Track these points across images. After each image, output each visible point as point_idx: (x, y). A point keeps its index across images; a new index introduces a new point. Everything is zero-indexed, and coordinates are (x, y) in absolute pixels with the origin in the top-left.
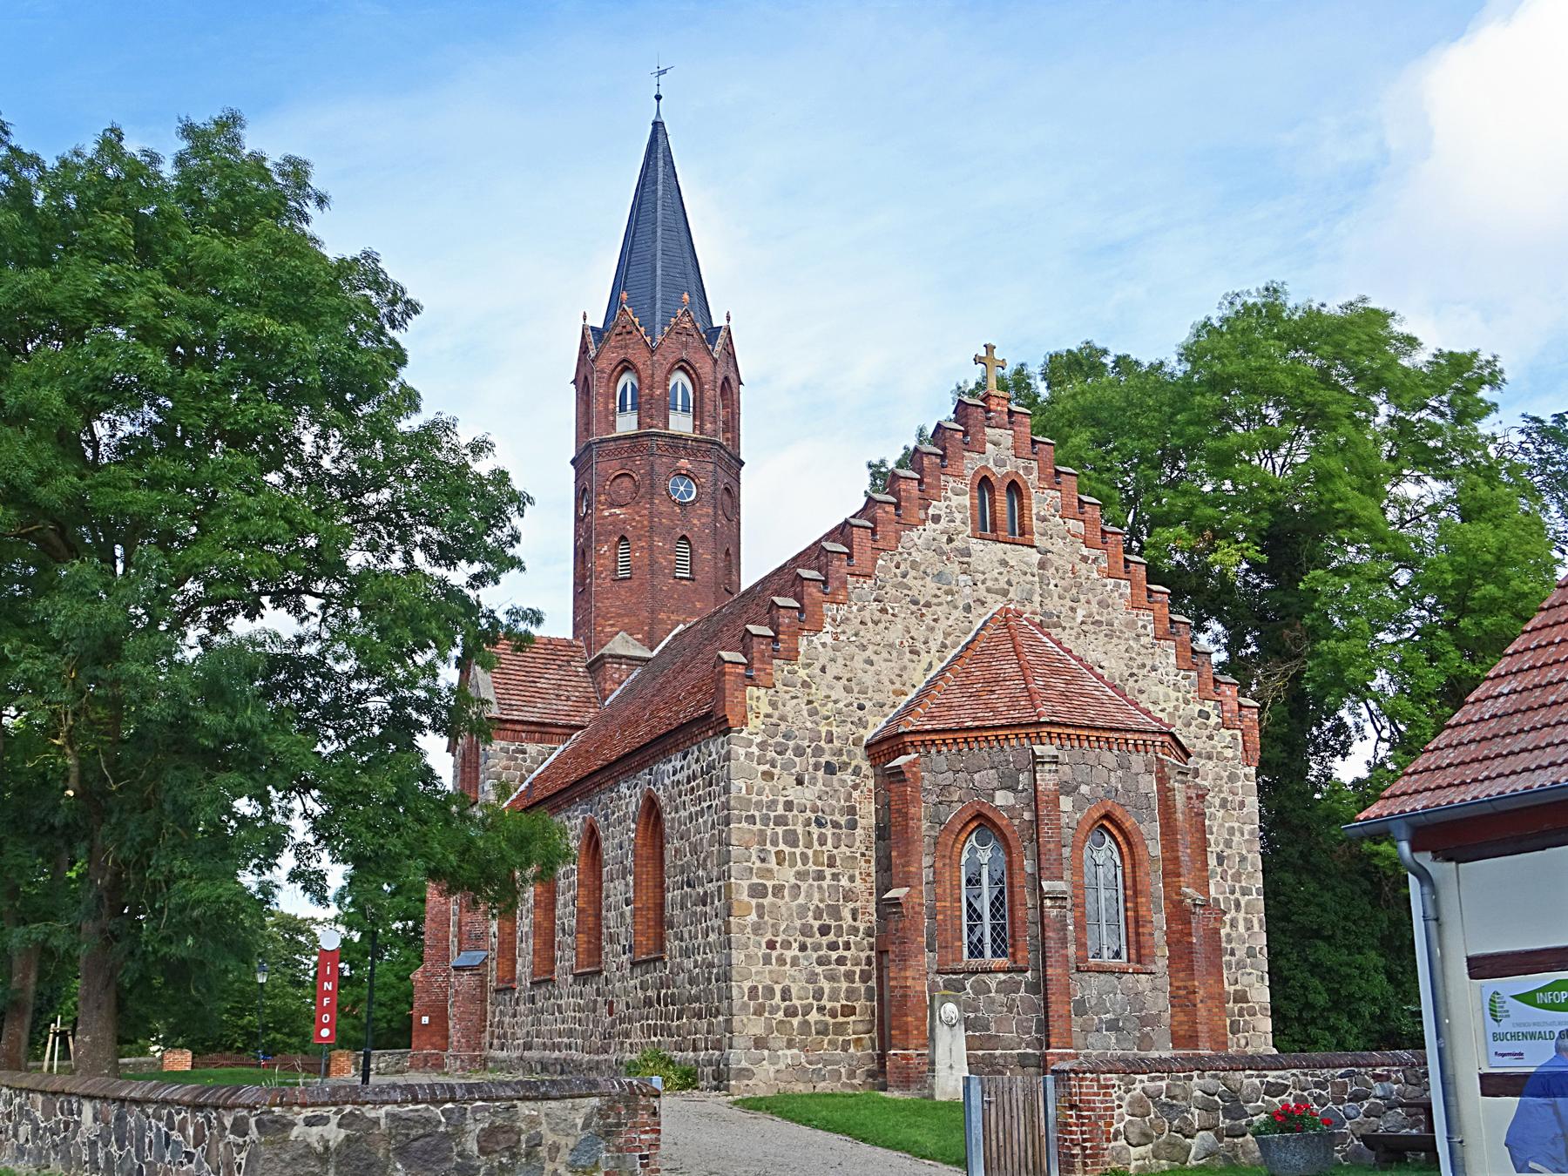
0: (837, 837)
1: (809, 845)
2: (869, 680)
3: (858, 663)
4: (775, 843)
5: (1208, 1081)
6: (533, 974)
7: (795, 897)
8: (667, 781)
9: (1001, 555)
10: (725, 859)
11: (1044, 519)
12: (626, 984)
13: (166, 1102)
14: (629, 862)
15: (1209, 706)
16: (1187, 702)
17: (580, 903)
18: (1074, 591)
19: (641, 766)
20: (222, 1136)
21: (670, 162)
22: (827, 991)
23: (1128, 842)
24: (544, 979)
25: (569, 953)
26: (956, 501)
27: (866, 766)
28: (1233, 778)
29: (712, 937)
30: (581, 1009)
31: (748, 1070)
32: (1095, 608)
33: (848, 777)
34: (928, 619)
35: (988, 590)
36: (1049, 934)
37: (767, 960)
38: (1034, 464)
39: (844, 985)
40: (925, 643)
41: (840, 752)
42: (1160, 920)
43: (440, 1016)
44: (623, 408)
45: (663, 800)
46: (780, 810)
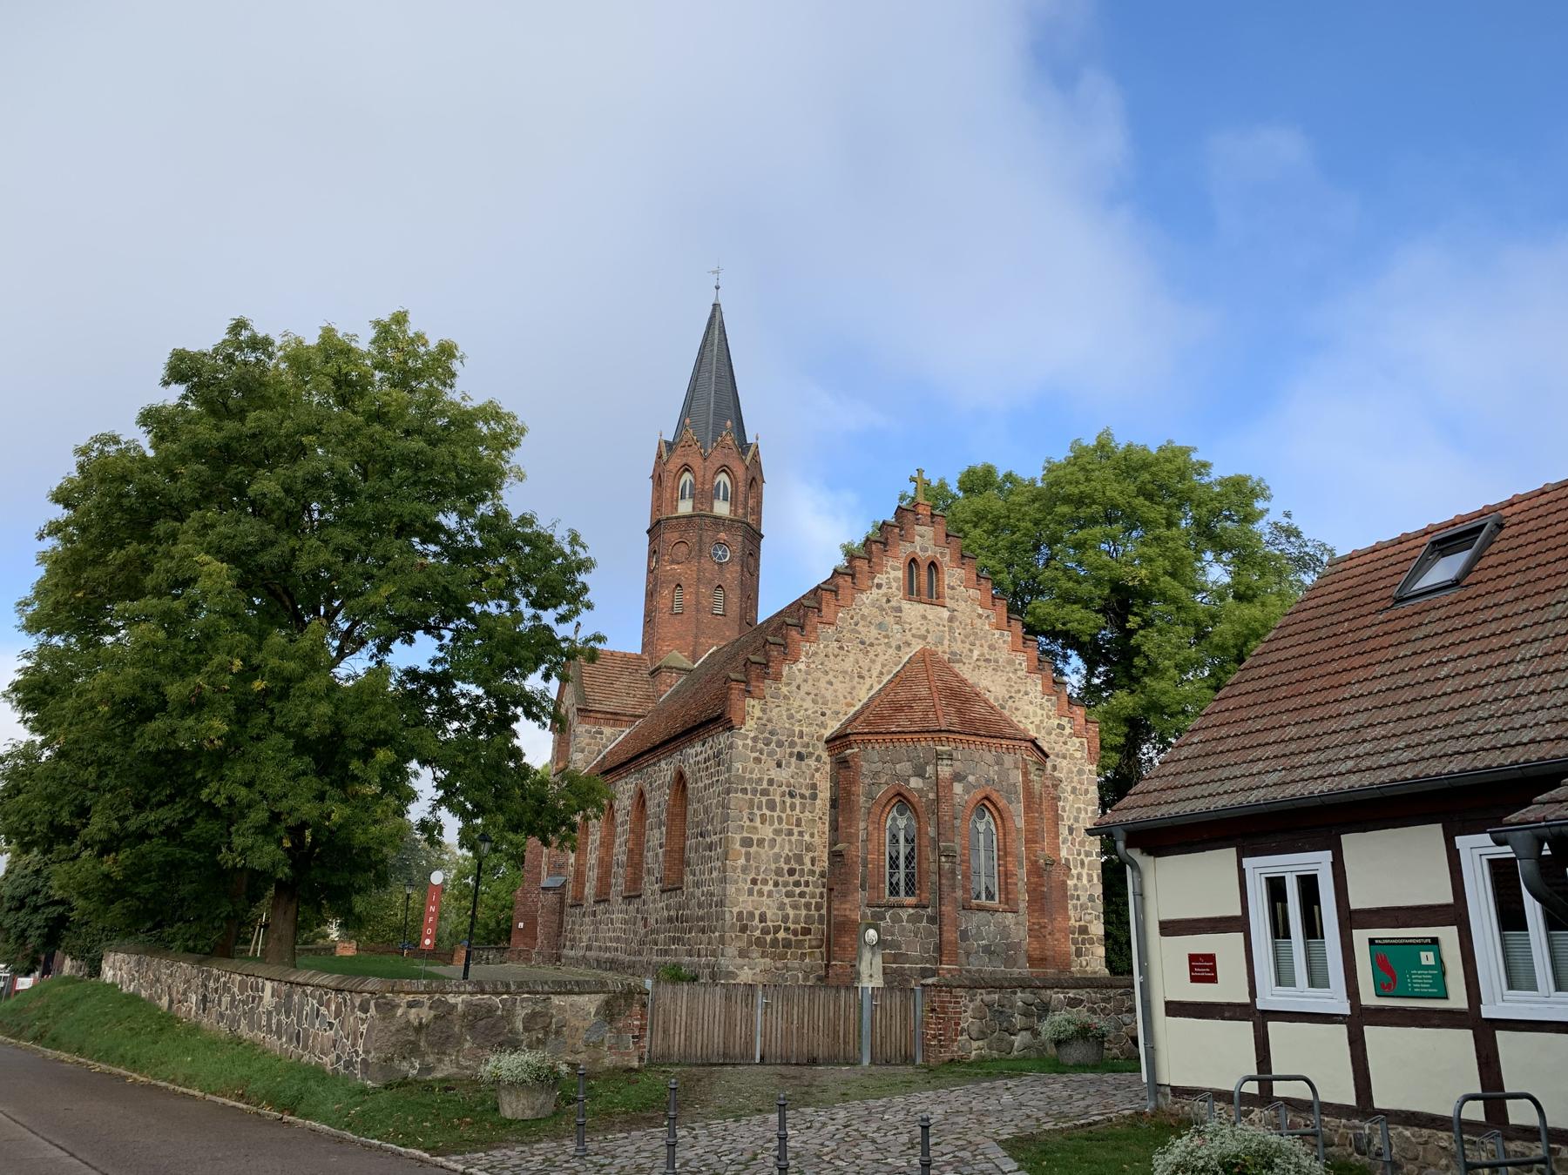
0: (803, 806)
1: (783, 810)
2: (829, 695)
3: (822, 684)
4: (760, 808)
7: (772, 847)
10: (726, 818)
11: (953, 588)
12: (657, 906)
13: (318, 986)
14: (664, 817)
15: (1064, 721)
16: (1049, 717)
23: (1001, 816)
25: (620, 880)
26: (893, 574)
27: (825, 756)
28: (1080, 772)
29: (715, 874)
30: (626, 922)
32: (986, 650)
33: (812, 762)
34: (871, 655)
37: (750, 892)
39: (804, 912)
41: (807, 745)
42: (1023, 873)
43: (532, 924)
46: (765, 785)
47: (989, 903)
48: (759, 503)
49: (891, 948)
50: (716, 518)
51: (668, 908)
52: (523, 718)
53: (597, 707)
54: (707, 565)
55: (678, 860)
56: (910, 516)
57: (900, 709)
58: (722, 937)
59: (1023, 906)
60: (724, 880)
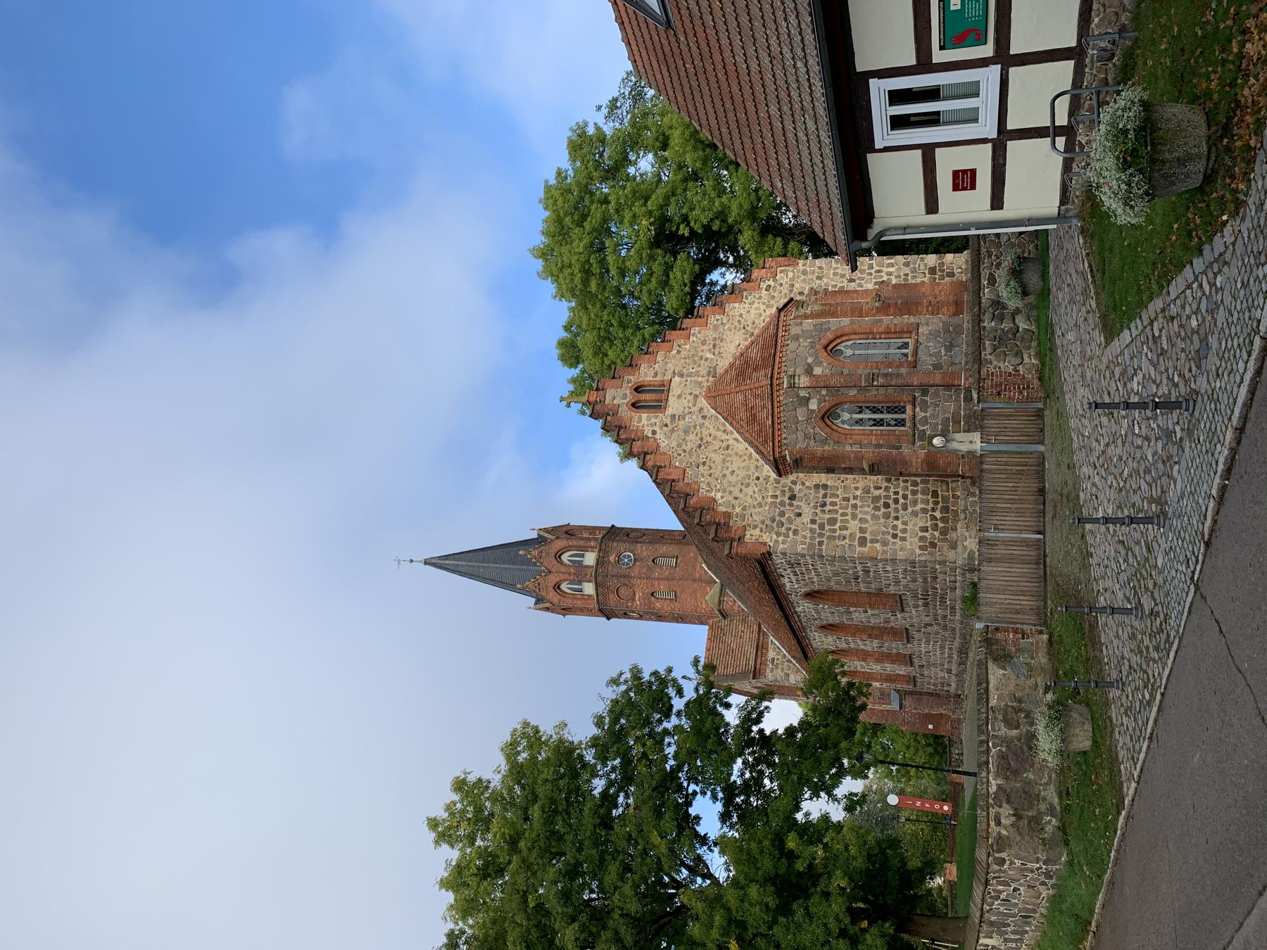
0: (833, 495)
1: (836, 512)
2: (742, 474)
3: (733, 479)
4: (834, 531)
5: (987, 317)
6: (906, 665)
7: (866, 521)
12: (914, 615)
13: (983, 900)
15: (764, 285)
16: (760, 298)
17: (865, 637)
19: (786, 599)
20: (1004, 872)
21: (447, 557)
23: (840, 336)
26: (644, 421)
27: (792, 477)
28: (805, 273)
29: (889, 568)
32: (706, 347)
33: (797, 488)
34: (710, 439)
37: (904, 539)
39: (919, 496)
41: (783, 492)
42: (886, 320)
43: (930, 718)
45: (807, 589)
46: (816, 526)
47: (911, 347)
49: (948, 426)
51: (916, 606)
52: (761, 726)
53: (752, 663)
55: (877, 598)
56: (598, 407)
57: (754, 417)
59: (912, 319)
60: (894, 561)
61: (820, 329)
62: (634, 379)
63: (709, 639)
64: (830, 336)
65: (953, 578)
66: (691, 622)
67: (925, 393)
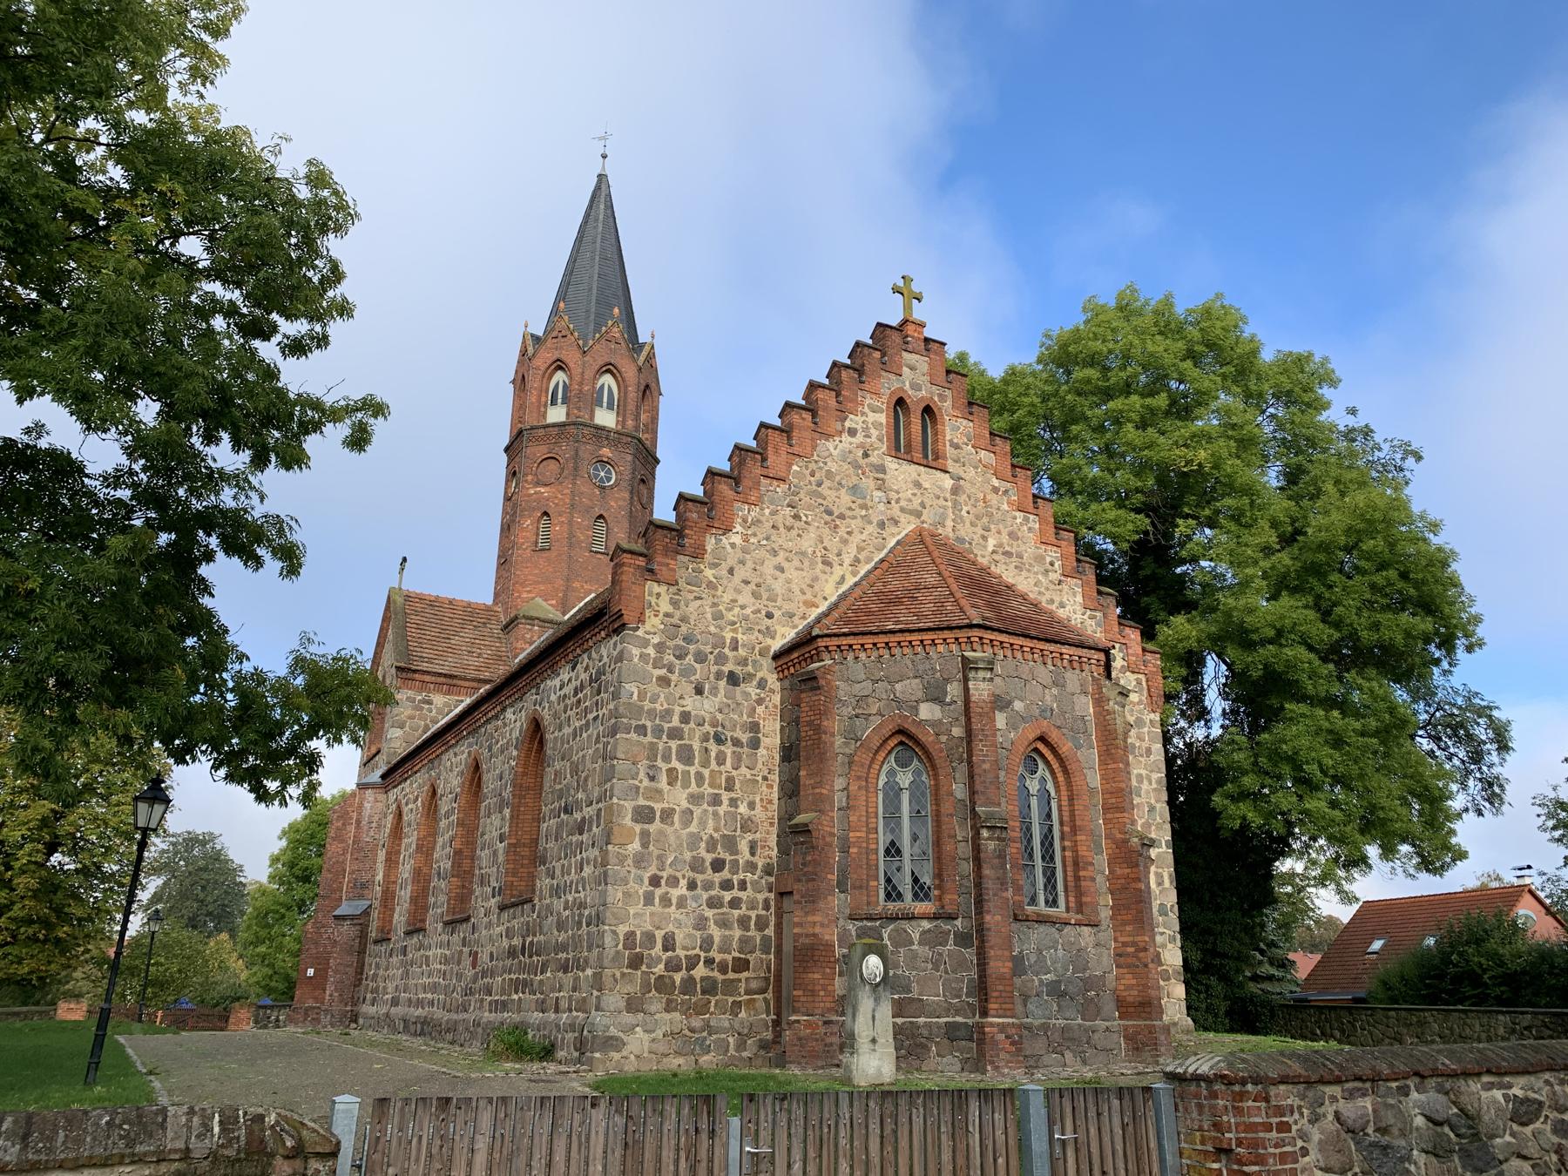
0: (738, 759)
1: (706, 764)
2: (778, 587)
4: (667, 759)
7: (687, 823)
8: (553, 698)
9: (914, 475)
10: (609, 775)
11: (957, 447)
12: (494, 931)
14: (507, 793)
18: (985, 520)
22: (717, 940)
23: (1064, 767)
24: (416, 928)
25: (442, 898)
26: (872, 417)
27: (773, 680)
29: (587, 871)
31: (617, 1039)
32: (1005, 539)
34: (842, 531)
35: (902, 510)
36: (987, 872)
37: (649, 899)
38: (948, 392)
39: (737, 933)
40: (839, 555)
42: (1102, 862)
44: (554, 403)
46: (676, 721)
47: (1051, 911)
48: (654, 419)
50: (598, 428)
51: (509, 934)
52: (220, 555)
53: (425, 666)
54: (584, 487)
55: (527, 855)
56: (896, 337)
57: (898, 601)
58: (598, 977)
59: (1105, 914)
60: (603, 879)
61: (1077, 727)
62: (947, 407)
63: (469, 605)
64: (1065, 748)
65: (564, 1004)
66: (498, 578)
67: (963, 939)
